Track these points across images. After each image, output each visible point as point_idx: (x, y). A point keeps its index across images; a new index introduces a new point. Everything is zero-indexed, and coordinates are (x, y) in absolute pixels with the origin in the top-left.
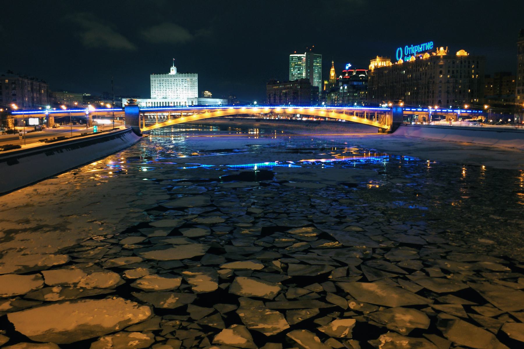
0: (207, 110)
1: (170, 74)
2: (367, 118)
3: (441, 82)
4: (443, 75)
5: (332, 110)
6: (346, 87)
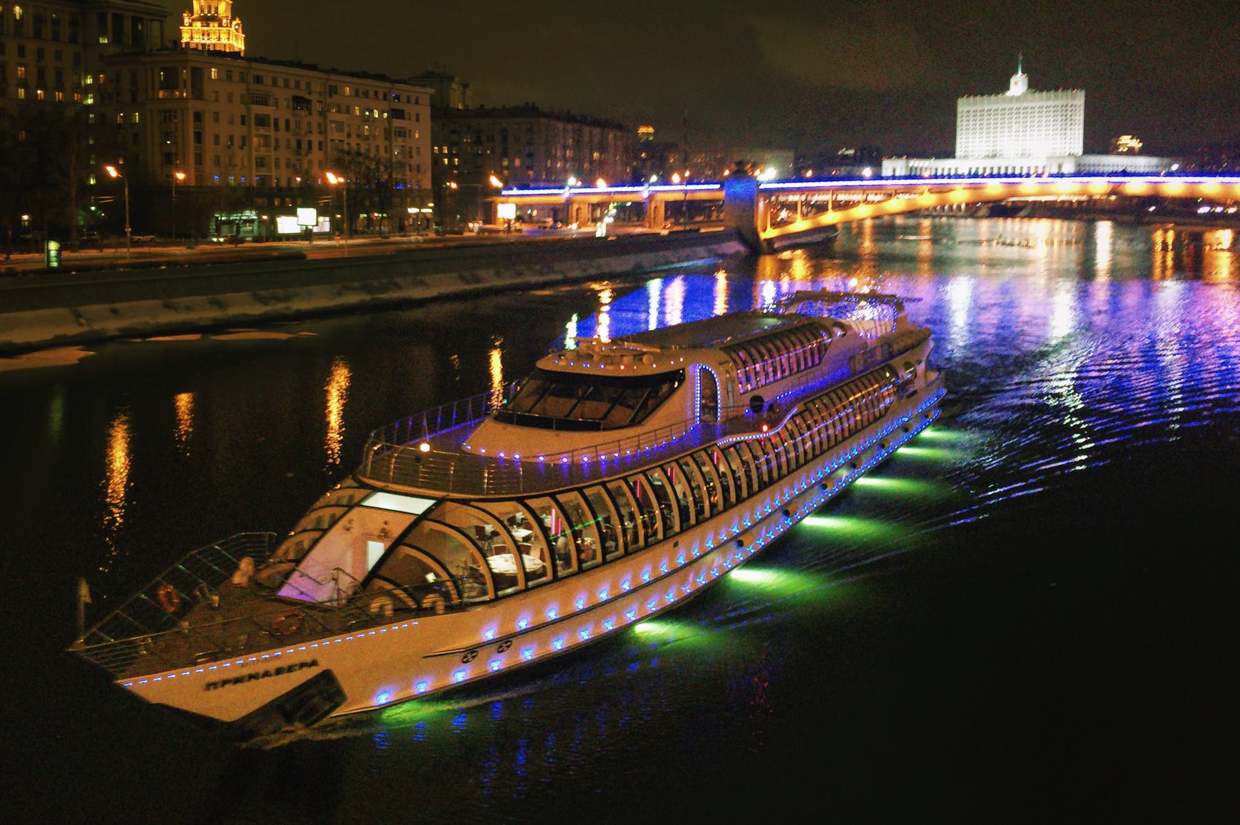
0: (929, 187)
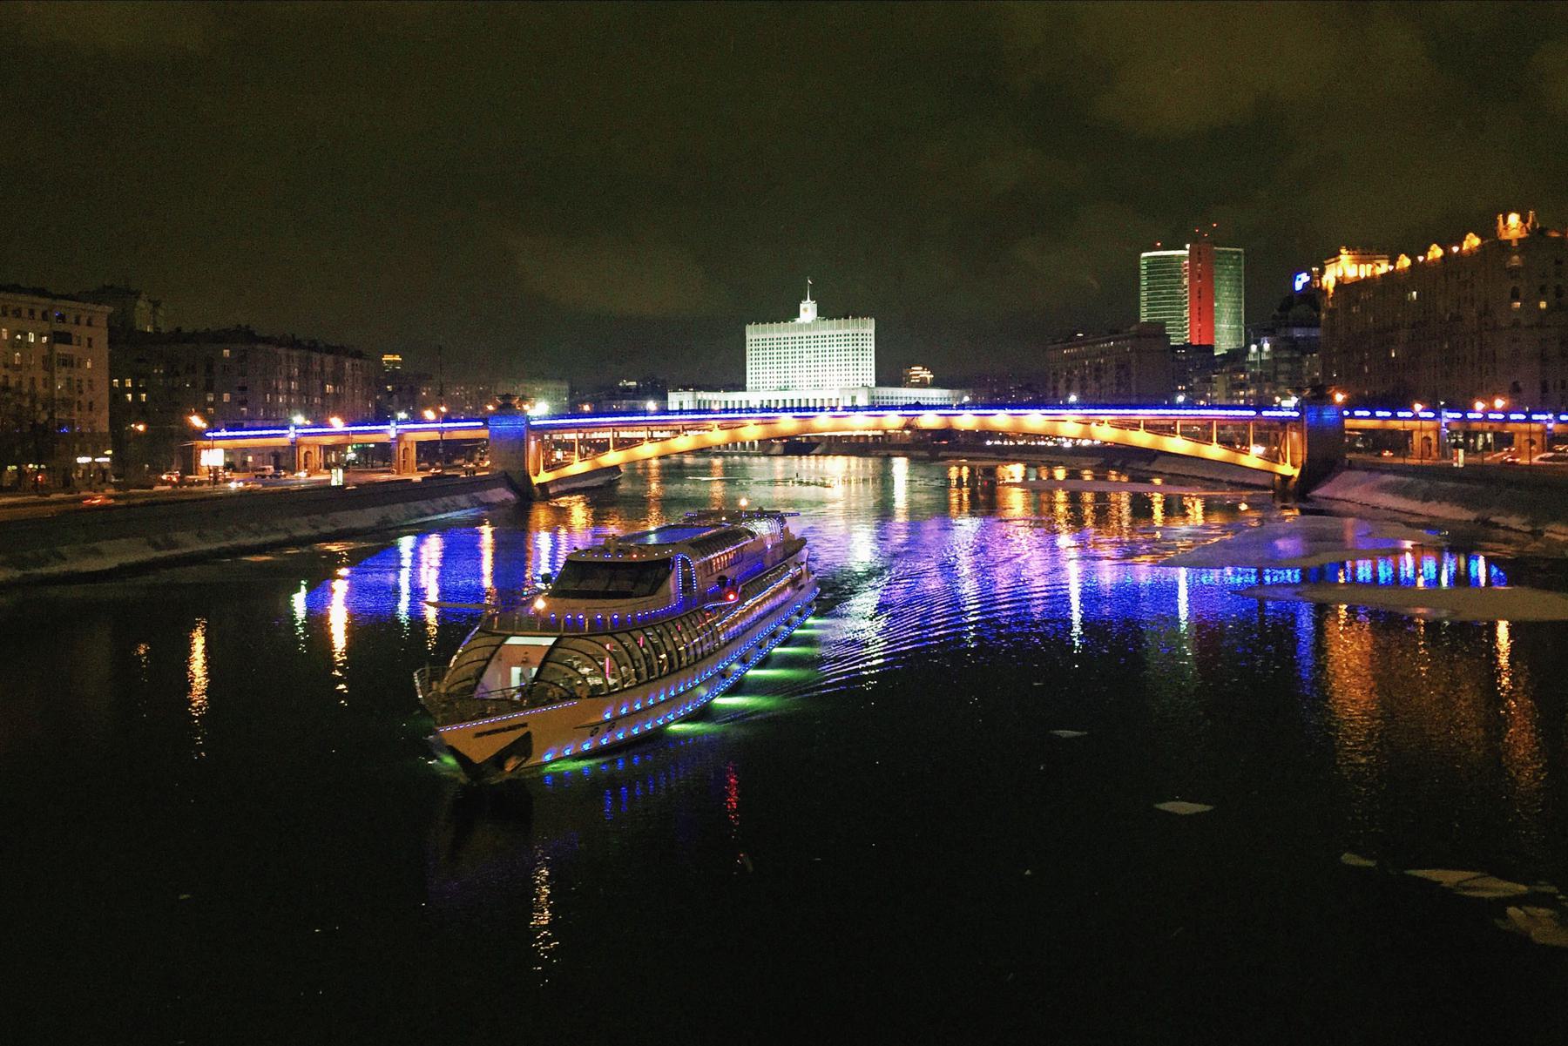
0: (719, 422)
1: (798, 320)
2: (1220, 442)
3: (1516, 324)
4: (1524, 301)
5: (1102, 418)
6: (1267, 347)
